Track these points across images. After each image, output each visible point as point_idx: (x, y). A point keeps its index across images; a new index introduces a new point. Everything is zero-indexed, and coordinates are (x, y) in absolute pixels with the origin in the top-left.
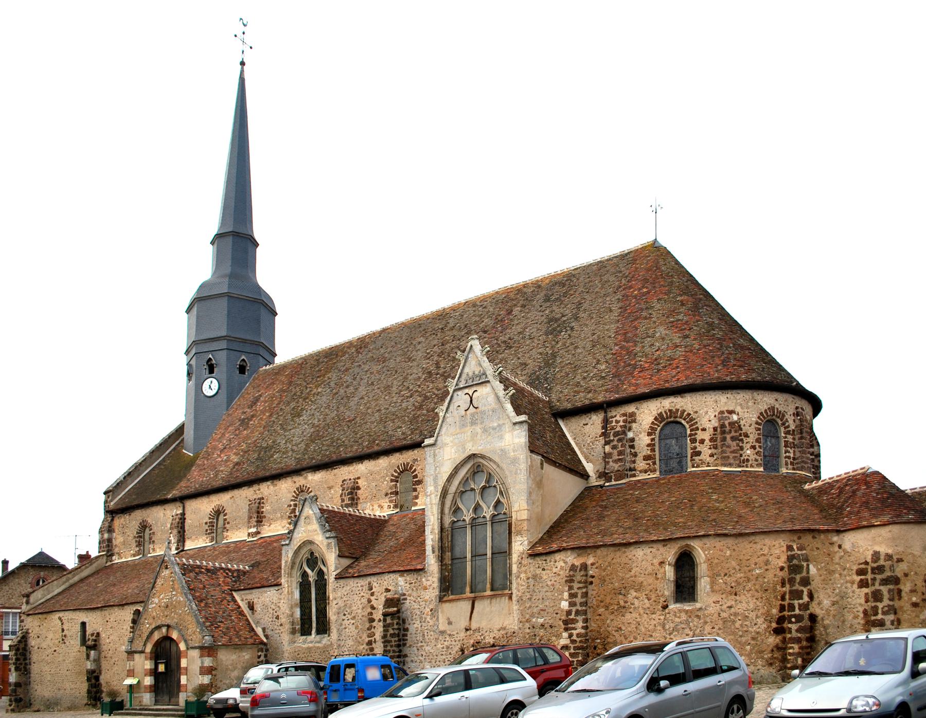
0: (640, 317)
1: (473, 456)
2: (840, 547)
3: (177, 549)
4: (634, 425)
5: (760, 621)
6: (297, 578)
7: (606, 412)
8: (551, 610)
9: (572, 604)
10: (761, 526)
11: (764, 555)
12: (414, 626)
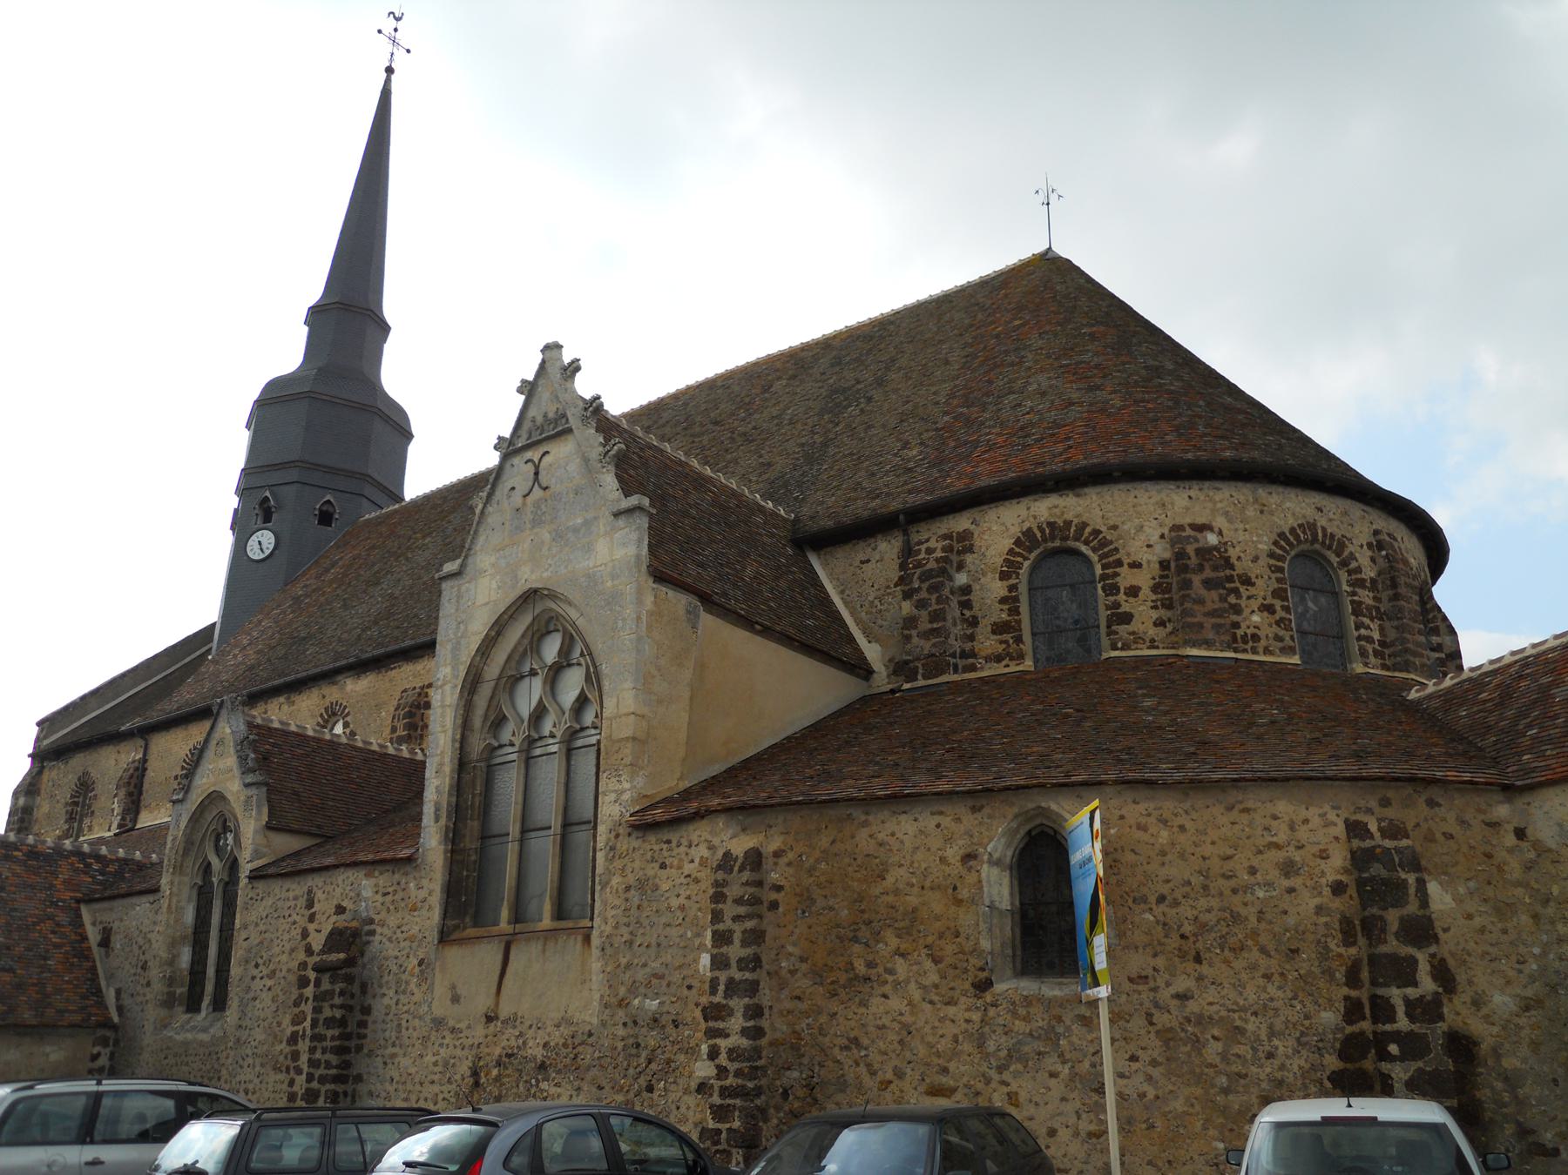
0: (1002, 365)
1: (530, 596)
2: (1520, 833)
3: (120, 826)
4: (969, 558)
5: (1283, 1046)
6: (191, 878)
7: (906, 533)
8: (676, 977)
9: (719, 963)
10: (1260, 766)
11: (1277, 846)
12: (384, 1002)
